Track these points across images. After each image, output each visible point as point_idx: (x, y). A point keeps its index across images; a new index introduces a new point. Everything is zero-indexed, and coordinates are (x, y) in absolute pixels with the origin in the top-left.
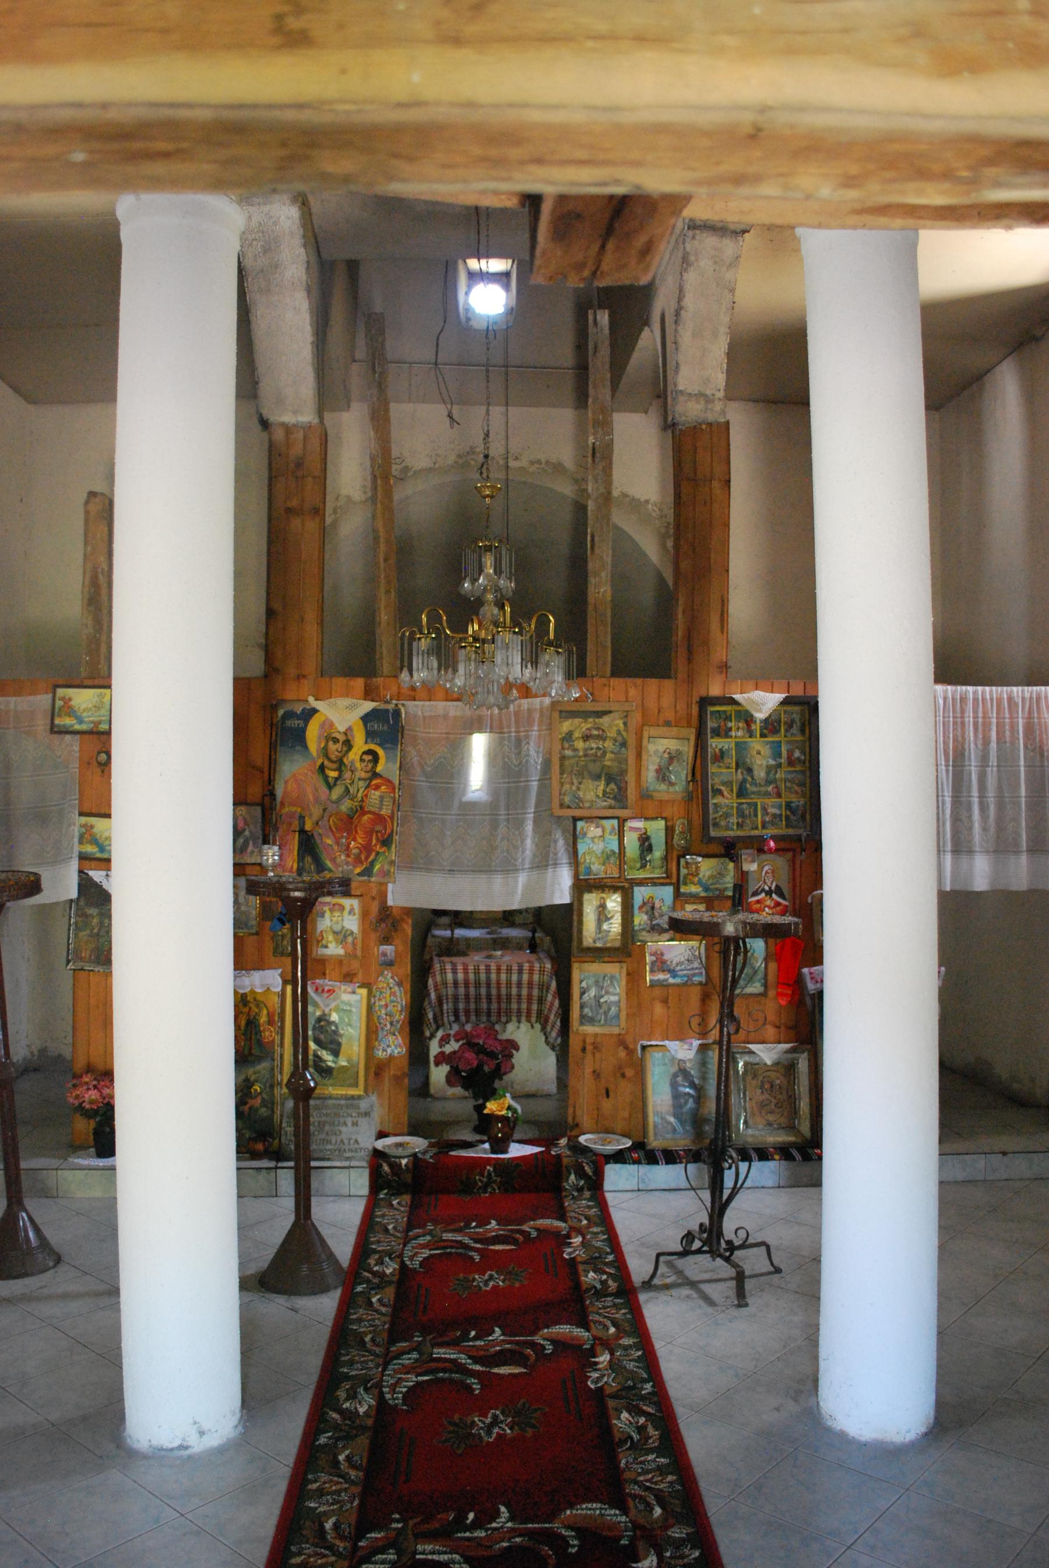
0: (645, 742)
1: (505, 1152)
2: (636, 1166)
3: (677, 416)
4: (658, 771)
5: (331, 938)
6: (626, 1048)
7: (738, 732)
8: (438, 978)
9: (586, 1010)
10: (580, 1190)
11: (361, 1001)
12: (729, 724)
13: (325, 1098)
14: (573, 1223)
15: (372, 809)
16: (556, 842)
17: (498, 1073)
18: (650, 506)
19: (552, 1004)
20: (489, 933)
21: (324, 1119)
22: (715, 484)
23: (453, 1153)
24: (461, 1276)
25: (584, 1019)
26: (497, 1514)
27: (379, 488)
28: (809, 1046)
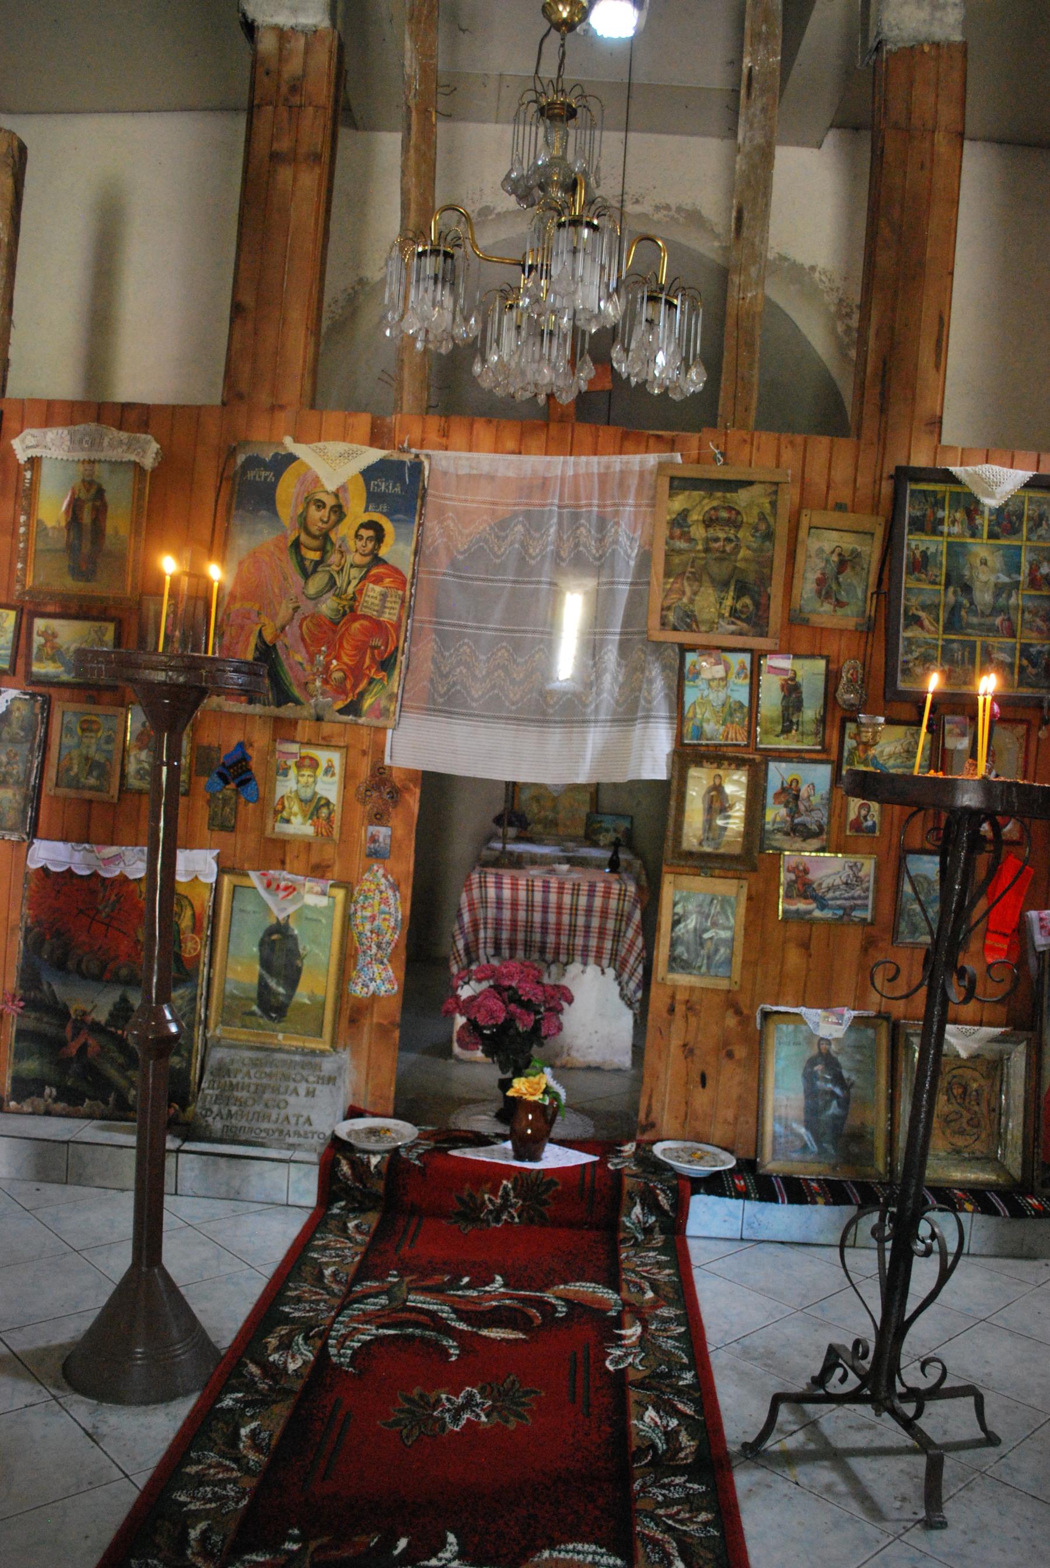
0: (803, 533)
1: (535, 1157)
2: (741, 1201)
3: (886, 28)
4: (820, 582)
5: (296, 808)
6: (738, 1012)
7: (953, 527)
8: (476, 893)
9: (680, 950)
10: (648, 1231)
11: (332, 907)
12: (940, 514)
13: (274, 1050)
14: (629, 1294)
15: (369, 612)
16: (650, 682)
17: (535, 1035)
18: (817, 275)
19: (633, 944)
20: (563, 851)
21: (264, 1081)
22: (940, 137)
23: (454, 1153)
24: (416, 1391)
25: (675, 962)
26: (443, 1544)
27: (414, 128)
28: (1030, 1035)
